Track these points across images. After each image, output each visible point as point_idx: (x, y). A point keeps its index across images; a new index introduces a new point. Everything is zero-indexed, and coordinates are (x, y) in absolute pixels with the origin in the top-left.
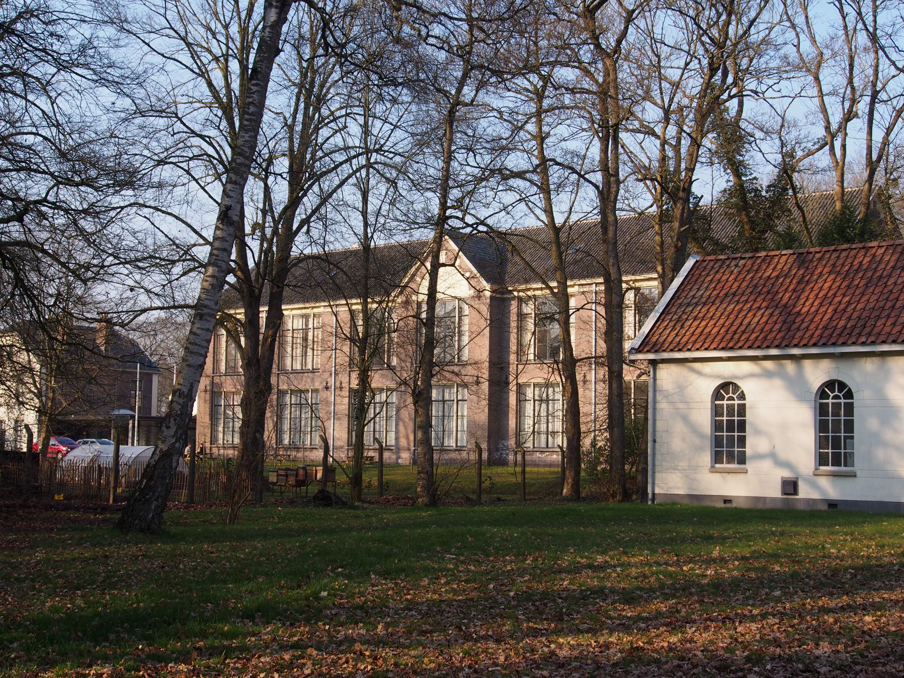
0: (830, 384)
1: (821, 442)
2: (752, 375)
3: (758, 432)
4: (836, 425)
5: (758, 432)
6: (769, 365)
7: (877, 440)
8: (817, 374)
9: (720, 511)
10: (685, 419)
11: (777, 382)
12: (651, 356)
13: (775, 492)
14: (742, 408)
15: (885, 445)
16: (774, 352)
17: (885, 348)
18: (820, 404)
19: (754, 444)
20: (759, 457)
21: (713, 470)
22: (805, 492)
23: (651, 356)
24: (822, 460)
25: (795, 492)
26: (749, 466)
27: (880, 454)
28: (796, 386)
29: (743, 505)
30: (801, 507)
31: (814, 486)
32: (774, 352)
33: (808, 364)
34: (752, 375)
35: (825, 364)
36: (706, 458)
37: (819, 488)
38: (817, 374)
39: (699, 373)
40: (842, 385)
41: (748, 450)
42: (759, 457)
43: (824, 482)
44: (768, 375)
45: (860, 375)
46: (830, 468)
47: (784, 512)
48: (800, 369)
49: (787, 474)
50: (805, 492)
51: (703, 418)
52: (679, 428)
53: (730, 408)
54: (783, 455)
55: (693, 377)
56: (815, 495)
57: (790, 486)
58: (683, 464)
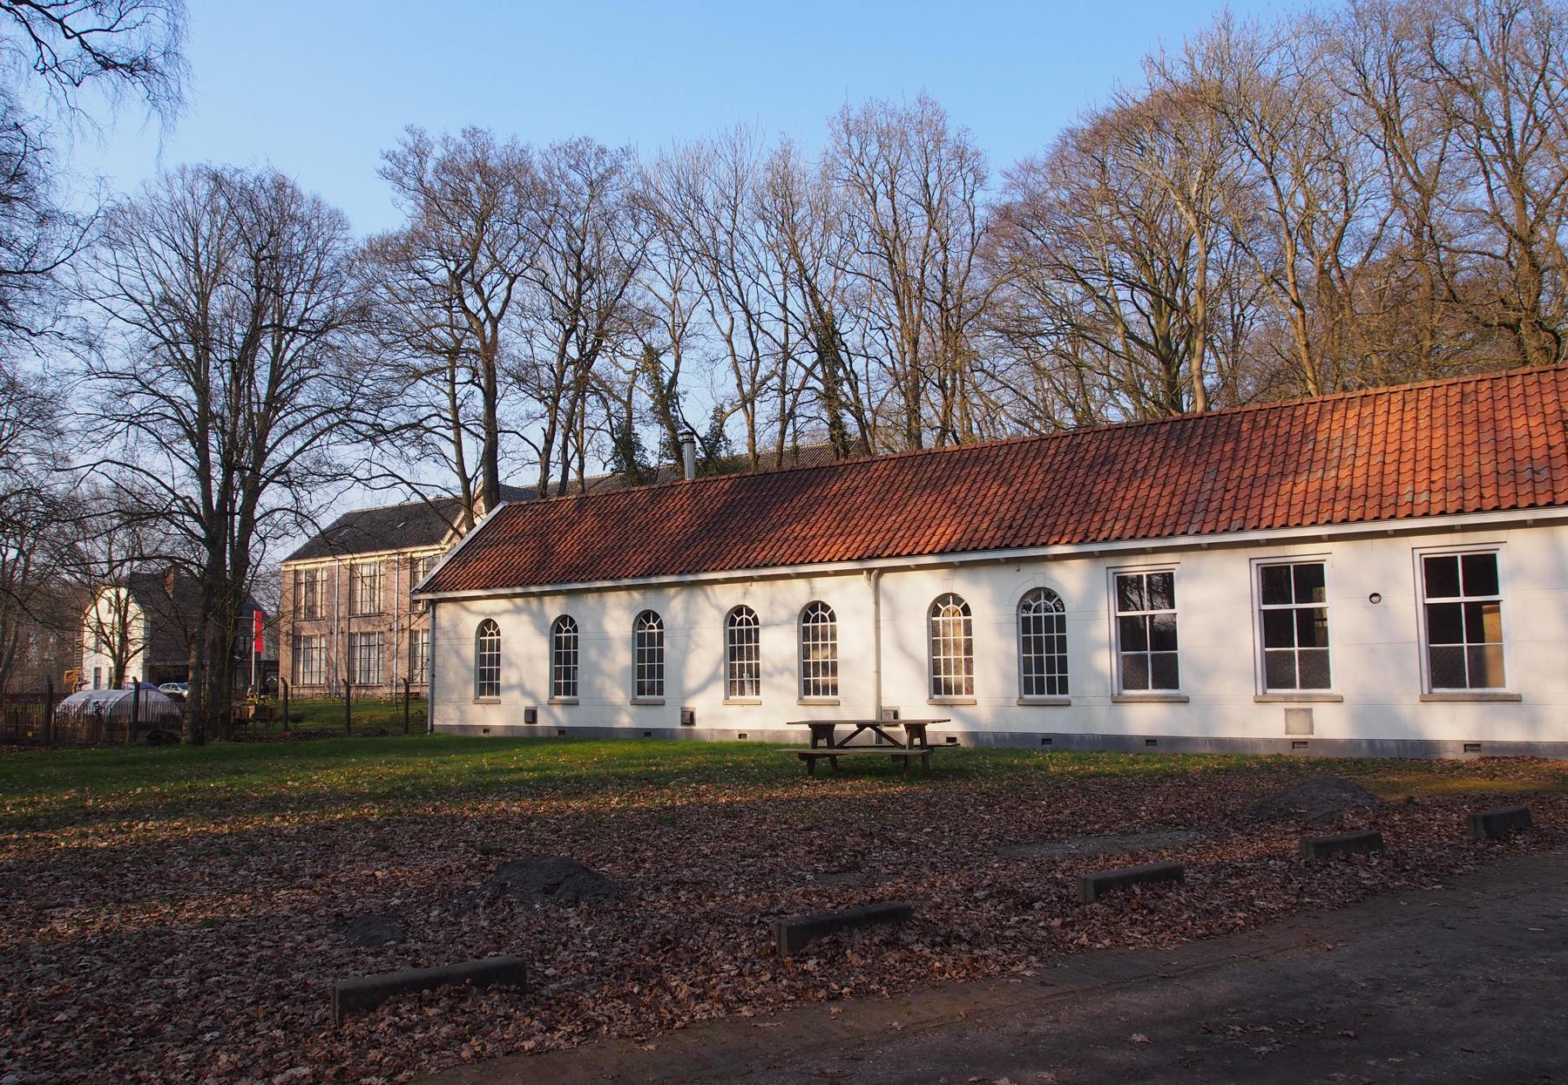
0: (943, 599)
1: (556, 674)
2: (506, 612)
3: (510, 664)
4: (1459, 631)
5: (510, 664)
6: (519, 601)
7: (596, 670)
8: (554, 608)
9: (481, 739)
10: (458, 653)
11: (525, 618)
12: (430, 596)
13: (521, 722)
14: (1062, 620)
15: (601, 672)
16: (519, 590)
17: (598, 584)
18: (1429, 606)
19: (507, 676)
20: (511, 687)
21: (476, 701)
22: (543, 721)
23: (430, 596)
24: (556, 690)
25: (534, 720)
26: (503, 697)
27: (598, 681)
28: (538, 618)
29: (500, 733)
30: (540, 734)
31: (551, 714)
32: (519, 590)
33: (547, 599)
34: (506, 612)
35: (560, 599)
36: (471, 690)
37: (554, 717)
38: (554, 608)
39: (467, 610)
40: (958, 600)
41: (502, 682)
42: (511, 687)
43: (557, 710)
44: (518, 611)
45: (583, 610)
46: (563, 697)
47: (527, 737)
48: (542, 604)
49: (530, 703)
50: (543, 721)
51: (470, 651)
52: (454, 661)
53: (651, 635)
54: (528, 686)
55: (464, 614)
56: (551, 724)
57: (531, 715)
58: (455, 697)
